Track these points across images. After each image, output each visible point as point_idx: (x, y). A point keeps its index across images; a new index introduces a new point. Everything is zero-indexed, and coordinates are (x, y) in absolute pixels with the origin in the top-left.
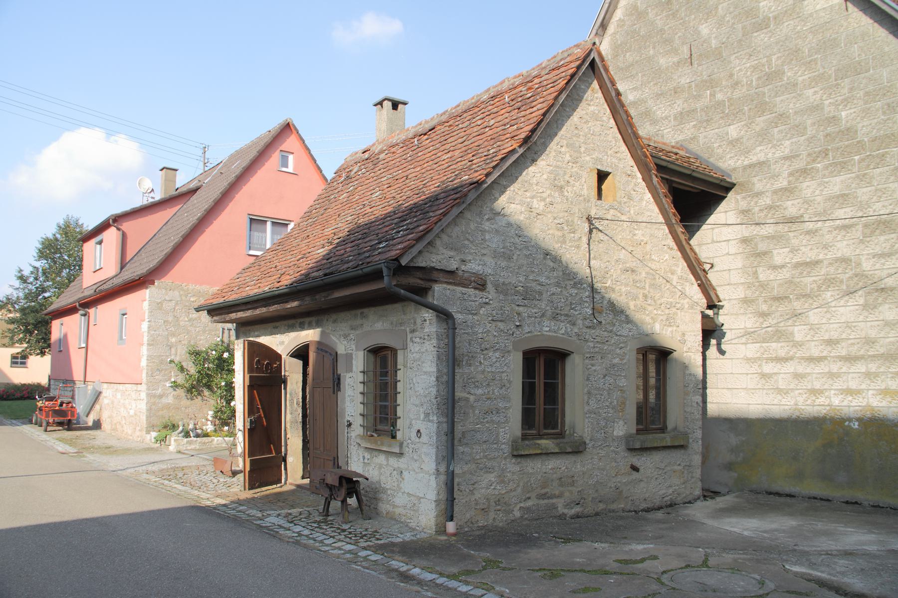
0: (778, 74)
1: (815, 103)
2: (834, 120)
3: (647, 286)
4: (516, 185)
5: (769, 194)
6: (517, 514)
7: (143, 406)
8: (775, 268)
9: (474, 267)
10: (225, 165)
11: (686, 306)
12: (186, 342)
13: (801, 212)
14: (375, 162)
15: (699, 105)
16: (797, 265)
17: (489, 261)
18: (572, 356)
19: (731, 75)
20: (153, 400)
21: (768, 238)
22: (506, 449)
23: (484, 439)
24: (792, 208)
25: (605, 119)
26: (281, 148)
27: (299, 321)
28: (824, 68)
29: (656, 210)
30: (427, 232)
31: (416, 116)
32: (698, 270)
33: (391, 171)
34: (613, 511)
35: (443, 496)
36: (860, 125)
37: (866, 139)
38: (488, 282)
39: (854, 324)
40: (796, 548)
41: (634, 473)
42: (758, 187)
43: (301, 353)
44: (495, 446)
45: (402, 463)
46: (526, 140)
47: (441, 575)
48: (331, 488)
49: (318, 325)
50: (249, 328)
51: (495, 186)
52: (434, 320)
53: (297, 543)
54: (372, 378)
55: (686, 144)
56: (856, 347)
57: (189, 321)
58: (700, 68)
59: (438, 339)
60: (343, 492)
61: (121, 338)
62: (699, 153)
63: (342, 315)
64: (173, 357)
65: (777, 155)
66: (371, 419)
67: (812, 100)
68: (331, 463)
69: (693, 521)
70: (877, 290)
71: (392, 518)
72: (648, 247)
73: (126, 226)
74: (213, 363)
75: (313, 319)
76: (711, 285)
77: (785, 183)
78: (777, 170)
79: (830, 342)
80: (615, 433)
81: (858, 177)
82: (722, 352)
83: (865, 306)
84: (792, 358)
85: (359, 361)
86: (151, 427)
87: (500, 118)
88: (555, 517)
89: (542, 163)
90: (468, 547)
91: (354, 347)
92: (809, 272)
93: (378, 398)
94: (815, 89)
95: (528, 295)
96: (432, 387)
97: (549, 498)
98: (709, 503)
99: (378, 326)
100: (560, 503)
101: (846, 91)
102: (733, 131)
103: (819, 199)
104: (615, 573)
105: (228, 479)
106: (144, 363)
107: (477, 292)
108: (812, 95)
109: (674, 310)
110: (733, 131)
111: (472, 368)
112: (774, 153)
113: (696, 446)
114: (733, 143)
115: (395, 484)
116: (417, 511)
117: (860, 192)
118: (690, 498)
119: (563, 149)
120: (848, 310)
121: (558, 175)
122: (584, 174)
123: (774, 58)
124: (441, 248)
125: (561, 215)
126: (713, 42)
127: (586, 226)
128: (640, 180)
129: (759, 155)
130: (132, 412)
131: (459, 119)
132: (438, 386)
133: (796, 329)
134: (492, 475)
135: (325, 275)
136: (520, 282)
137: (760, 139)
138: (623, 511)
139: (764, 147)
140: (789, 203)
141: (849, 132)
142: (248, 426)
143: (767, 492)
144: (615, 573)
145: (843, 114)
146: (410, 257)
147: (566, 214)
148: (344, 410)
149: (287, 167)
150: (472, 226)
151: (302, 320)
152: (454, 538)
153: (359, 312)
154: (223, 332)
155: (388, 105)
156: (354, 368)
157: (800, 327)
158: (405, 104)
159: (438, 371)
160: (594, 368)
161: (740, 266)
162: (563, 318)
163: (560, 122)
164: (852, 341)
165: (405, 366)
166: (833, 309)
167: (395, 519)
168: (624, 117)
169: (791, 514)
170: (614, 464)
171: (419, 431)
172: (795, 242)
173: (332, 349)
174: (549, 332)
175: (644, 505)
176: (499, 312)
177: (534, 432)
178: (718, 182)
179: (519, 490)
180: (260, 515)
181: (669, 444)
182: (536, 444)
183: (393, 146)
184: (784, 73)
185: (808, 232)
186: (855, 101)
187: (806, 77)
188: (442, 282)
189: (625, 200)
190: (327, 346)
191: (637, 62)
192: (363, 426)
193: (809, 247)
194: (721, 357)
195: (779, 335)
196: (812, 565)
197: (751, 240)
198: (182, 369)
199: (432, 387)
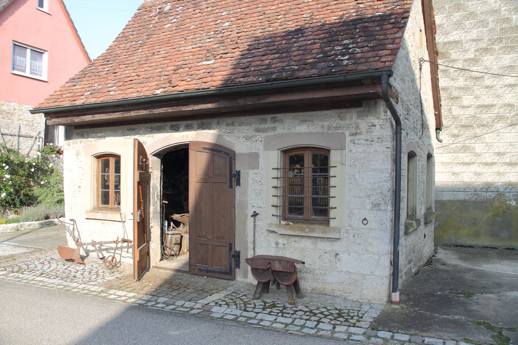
1: (495, 8)
2: (507, 20)
5: (461, 61)
8: (464, 107)
16: (479, 107)
21: (459, 88)
27: (170, 124)
39: (515, 144)
42: (454, 56)
45: (337, 247)
50: (88, 130)
65: (468, 38)
67: (493, 7)
75: (215, 121)
77: (472, 56)
79: (499, 154)
84: (473, 163)
85: (271, 161)
91: (262, 148)
92: (487, 111)
99: (302, 130)
103: (495, 67)
129: (455, 37)
135: (268, 81)
139: (459, 32)
143: (454, 245)
149: (42, 7)
151: (174, 123)
153: (269, 117)
164: (513, 154)
166: (502, 134)
172: (478, 92)
193: (487, 96)
195: (465, 149)
197: (448, 89)
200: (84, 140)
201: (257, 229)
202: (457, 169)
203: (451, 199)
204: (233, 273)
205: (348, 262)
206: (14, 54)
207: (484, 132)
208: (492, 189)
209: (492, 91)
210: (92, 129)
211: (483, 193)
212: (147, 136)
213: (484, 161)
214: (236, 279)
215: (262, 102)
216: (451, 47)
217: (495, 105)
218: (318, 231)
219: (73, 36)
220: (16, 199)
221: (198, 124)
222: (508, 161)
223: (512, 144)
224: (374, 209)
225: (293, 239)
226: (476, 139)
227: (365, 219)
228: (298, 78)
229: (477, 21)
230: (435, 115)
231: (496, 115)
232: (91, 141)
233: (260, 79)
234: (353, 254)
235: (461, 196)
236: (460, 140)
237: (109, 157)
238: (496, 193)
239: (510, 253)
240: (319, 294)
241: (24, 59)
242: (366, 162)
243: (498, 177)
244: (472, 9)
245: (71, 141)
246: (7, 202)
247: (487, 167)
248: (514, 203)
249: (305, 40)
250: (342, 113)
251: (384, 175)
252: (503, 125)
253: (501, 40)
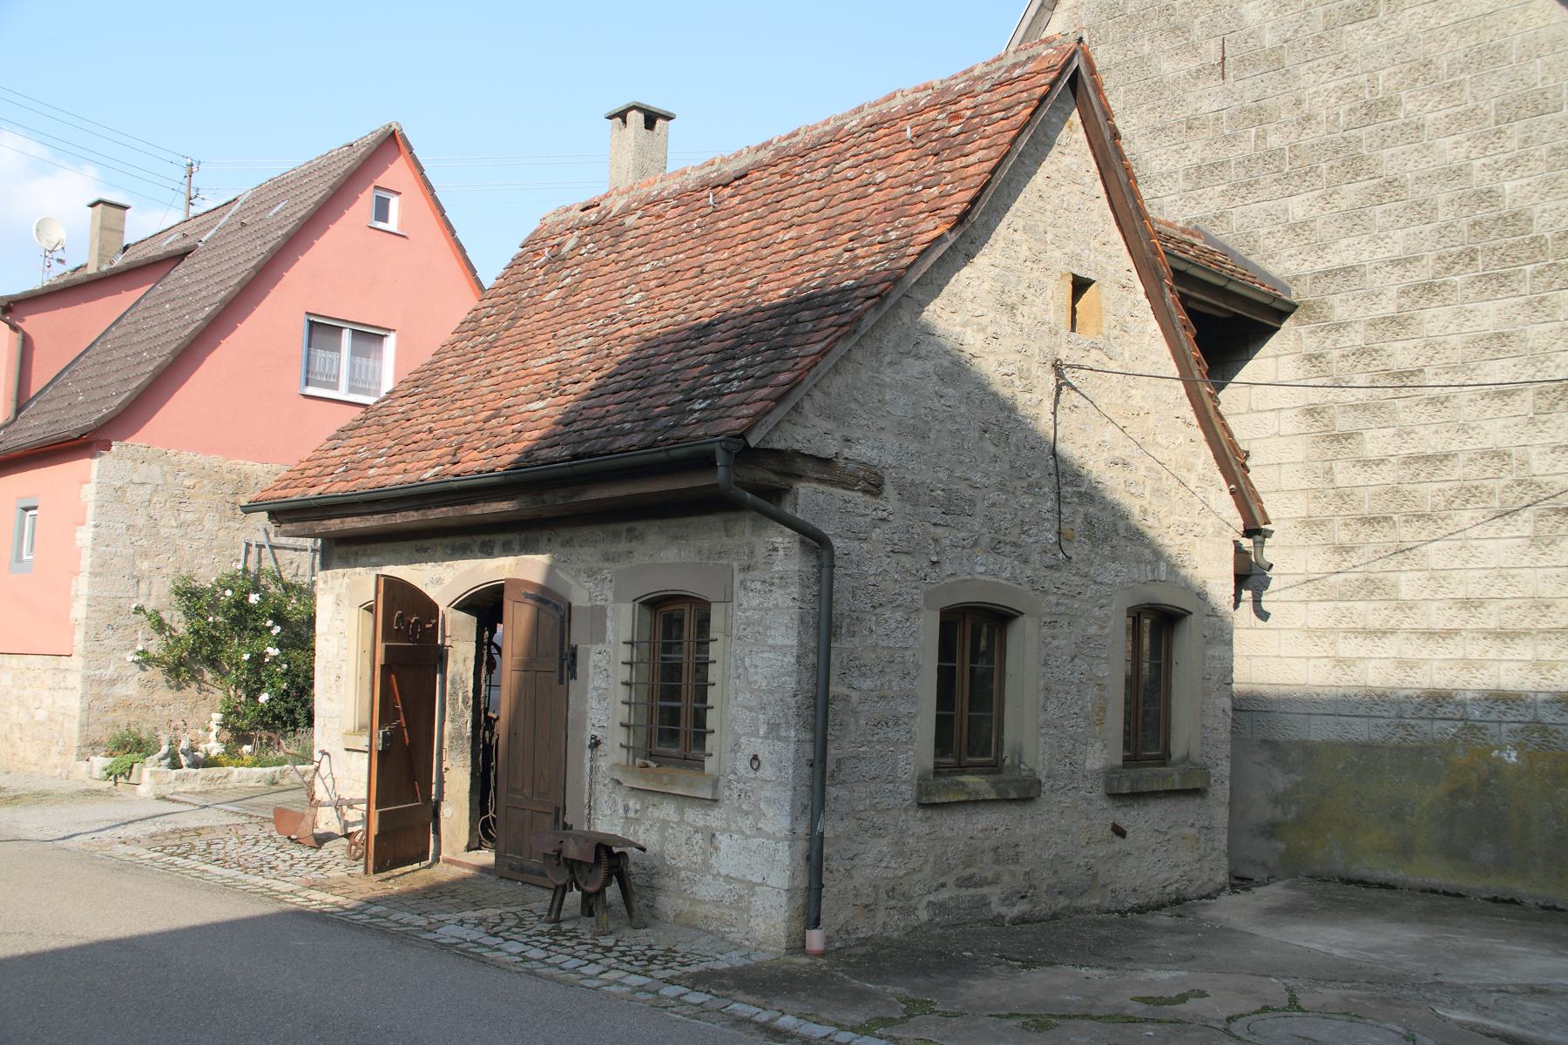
0: (1387, 105)
1: (1456, 163)
2: (1488, 196)
3: (1147, 493)
4: (937, 301)
5: (1360, 327)
6: (924, 915)
7: (73, 703)
8: (1366, 463)
9: (863, 451)
10: (249, 206)
11: (1211, 530)
12: (170, 570)
13: (1421, 362)
14: (617, 230)
15: (1233, 155)
16: (1410, 460)
17: (892, 442)
18: (1021, 619)
19: (1298, 103)
20: (95, 689)
21: (1355, 407)
22: (909, 791)
23: (873, 774)
24: (1402, 354)
25: (1088, 180)
26: (378, 182)
27: (480, 539)
28: (1476, 99)
29: (1167, 352)
30: (795, 384)
31: (692, 149)
32: (1231, 461)
33: (661, 253)
34: (1082, 911)
35: (802, 881)
36: (1539, 208)
37: (1547, 235)
38: (887, 480)
40: (1438, 978)
41: (1118, 839)
42: (1340, 312)
43: (486, 606)
44: (890, 786)
45: (715, 818)
46: (962, 219)
47: (840, 1027)
48: (572, 865)
50: (356, 548)
51: (905, 302)
52: (796, 547)
53: (531, 973)
54: (646, 655)
55: (1205, 226)
57: (180, 526)
58: (1239, 85)
59: (803, 586)
60: (601, 873)
61: (19, 558)
62: (1229, 244)
63: (585, 532)
64: (141, 601)
65: (1379, 256)
66: (642, 732)
67: (1449, 158)
68: (549, 820)
69: (1232, 930)
70: (1557, 511)
71: (689, 924)
72: (1152, 419)
73: (33, 323)
74: (225, 614)
76: (1254, 492)
77: (1391, 310)
78: (1378, 284)
79: (1467, 603)
80: (1088, 765)
81: (1529, 303)
82: (1263, 615)
83: (1534, 540)
84: (1393, 632)
85: (622, 622)
86: (91, 746)
87: (895, 170)
88: (986, 921)
89: (981, 260)
90: (857, 976)
91: (610, 596)
92: (1432, 474)
93: (657, 693)
94: (1457, 138)
95: (953, 507)
96: (788, 674)
97: (976, 885)
98: (1243, 897)
99: (669, 558)
100: (994, 894)
101: (1514, 143)
102: (1298, 207)
103: (1454, 340)
104: (1146, 1020)
105: (311, 852)
106: (79, 611)
107: (868, 498)
108: (1450, 149)
109: (1190, 536)
110: (1298, 207)
111: (857, 640)
112: (1373, 252)
113: (1220, 791)
114: (1296, 228)
115: (699, 859)
116: (747, 909)
117: (1532, 331)
118: (1209, 888)
119: (1017, 236)
120: (1502, 545)
121: (1005, 284)
122: (1051, 284)
123: (1382, 75)
124: (811, 416)
125: (1010, 358)
126: (1268, 36)
127: (1051, 378)
128: (1142, 296)
129: (1345, 254)
130: (41, 715)
131: (800, 161)
132: (799, 672)
133: (1403, 577)
134: (884, 841)
135: (575, 457)
136: (940, 481)
137: (1348, 224)
138: (1099, 911)
139: (1356, 240)
140: (1399, 345)
141: (1516, 219)
142: (378, 744)
143: (1341, 880)
144: (1146, 1020)
145: (1508, 186)
146: (765, 431)
147: (1019, 357)
148: (583, 715)
149: (385, 220)
150: (865, 375)
151: (487, 538)
152: (821, 961)
153: (623, 527)
154: (247, 552)
155: (636, 118)
156: (610, 636)
157: (1410, 574)
158: (668, 118)
159: (801, 644)
160: (1056, 643)
161: (1300, 457)
162: (1008, 549)
163: (1013, 184)
164: (1509, 603)
165: (727, 634)
166: (1475, 543)
167: (695, 927)
168: (1123, 178)
169: (1402, 920)
170: (1084, 823)
171: (755, 758)
172: (1405, 418)
173: (561, 599)
174: (984, 576)
175: (1132, 901)
176: (905, 537)
177: (951, 760)
178: (1267, 301)
179: (928, 869)
180: (423, 922)
181: (1177, 787)
182: (958, 783)
183: (655, 203)
184: (1399, 104)
185: (1432, 401)
186: (1531, 164)
187: (1442, 114)
188: (810, 479)
189: (1116, 332)
190: (554, 594)
191: (1117, 65)
192: (628, 748)
193: (1433, 428)
194: (1260, 623)
195: (1371, 588)
196: (1482, 1009)
197: (1324, 410)
198: (160, 626)
199: (788, 674)
200: (349, 571)
202: (1348, 648)
203: (1333, 737)
205: (731, 856)
206: (309, 346)
207: (1424, 535)
208: (1448, 710)
209: (1446, 413)
211: (1421, 722)
213: (1424, 626)
216: (1333, 286)
217: (1455, 456)
219: (465, 282)
220: (299, 710)
222: (1492, 624)
223: (1504, 572)
226: (1401, 557)
229: (1403, 204)
230: (1232, 493)
231: (1459, 484)
235: (1360, 731)
236: (1355, 561)
238: (1460, 724)
239: (1556, 920)
241: (334, 355)
243: (1465, 676)
244: (1388, 170)
246: (277, 717)
247: (1432, 644)
248: (1512, 757)
252: (1479, 514)
253: (1471, 256)
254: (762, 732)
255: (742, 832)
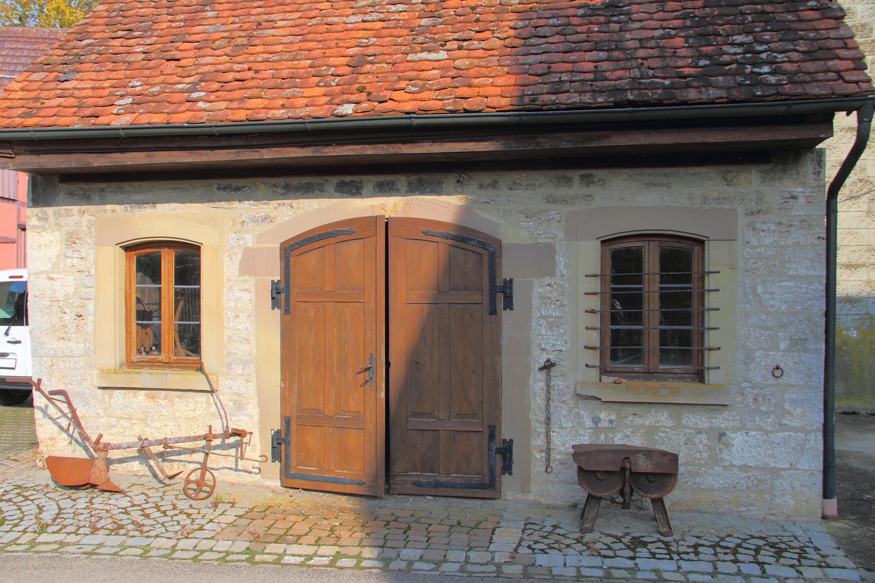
27: (335, 180)
39: (856, 231)
45: (721, 421)
49: (460, 186)
56: (857, 254)
75: (452, 178)
91: (561, 235)
135: (617, 105)
153: (575, 175)
164: (854, 248)
200: (92, 208)
201: (554, 394)
204: (497, 485)
205: (744, 448)
210: (115, 185)
212: (274, 203)
214: (503, 496)
215: (595, 144)
218: (688, 391)
221: (409, 184)
223: (851, 231)
224: (794, 349)
225: (630, 409)
227: (778, 368)
228: (685, 103)
232: (113, 211)
233: (600, 100)
234: (754, 433)
237: (159, 247)
240: (687, 511)
242: (777, 263)
245: (50, 210)
248: (854, 334)
249: (642, 28)
250: (730, 171)
251: (813, 287)
254: (782, 346)
255: (760, 429)
